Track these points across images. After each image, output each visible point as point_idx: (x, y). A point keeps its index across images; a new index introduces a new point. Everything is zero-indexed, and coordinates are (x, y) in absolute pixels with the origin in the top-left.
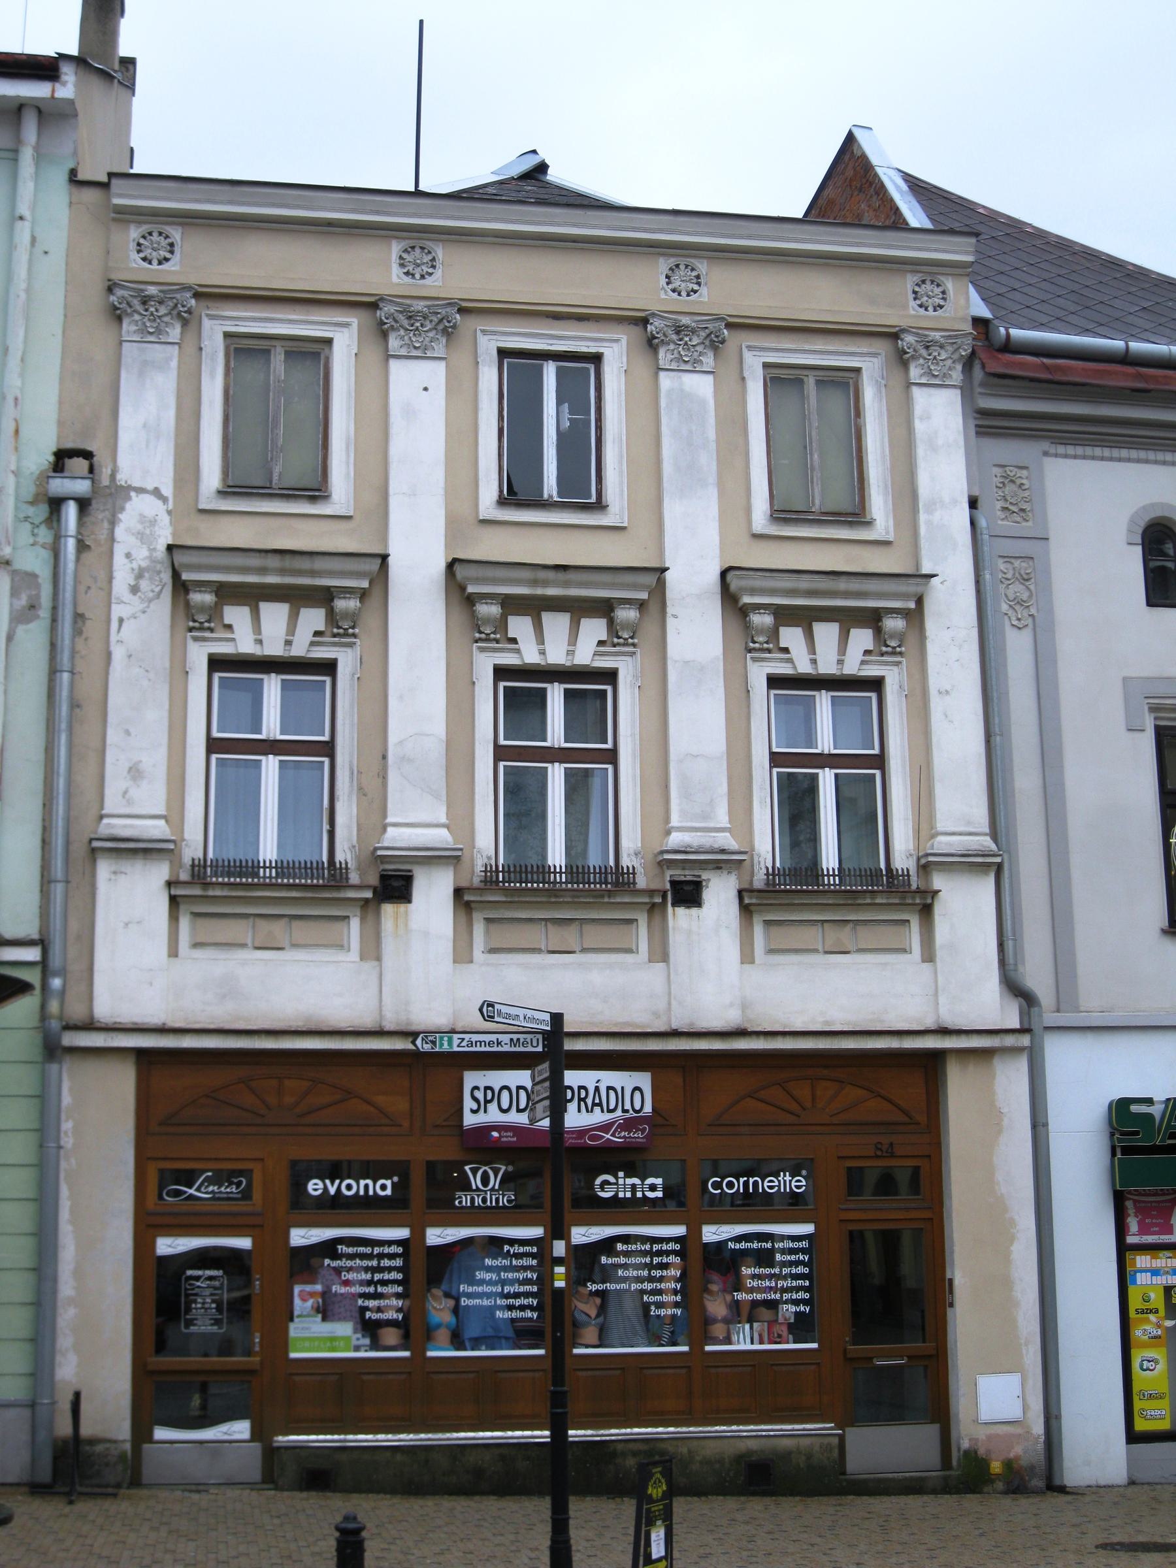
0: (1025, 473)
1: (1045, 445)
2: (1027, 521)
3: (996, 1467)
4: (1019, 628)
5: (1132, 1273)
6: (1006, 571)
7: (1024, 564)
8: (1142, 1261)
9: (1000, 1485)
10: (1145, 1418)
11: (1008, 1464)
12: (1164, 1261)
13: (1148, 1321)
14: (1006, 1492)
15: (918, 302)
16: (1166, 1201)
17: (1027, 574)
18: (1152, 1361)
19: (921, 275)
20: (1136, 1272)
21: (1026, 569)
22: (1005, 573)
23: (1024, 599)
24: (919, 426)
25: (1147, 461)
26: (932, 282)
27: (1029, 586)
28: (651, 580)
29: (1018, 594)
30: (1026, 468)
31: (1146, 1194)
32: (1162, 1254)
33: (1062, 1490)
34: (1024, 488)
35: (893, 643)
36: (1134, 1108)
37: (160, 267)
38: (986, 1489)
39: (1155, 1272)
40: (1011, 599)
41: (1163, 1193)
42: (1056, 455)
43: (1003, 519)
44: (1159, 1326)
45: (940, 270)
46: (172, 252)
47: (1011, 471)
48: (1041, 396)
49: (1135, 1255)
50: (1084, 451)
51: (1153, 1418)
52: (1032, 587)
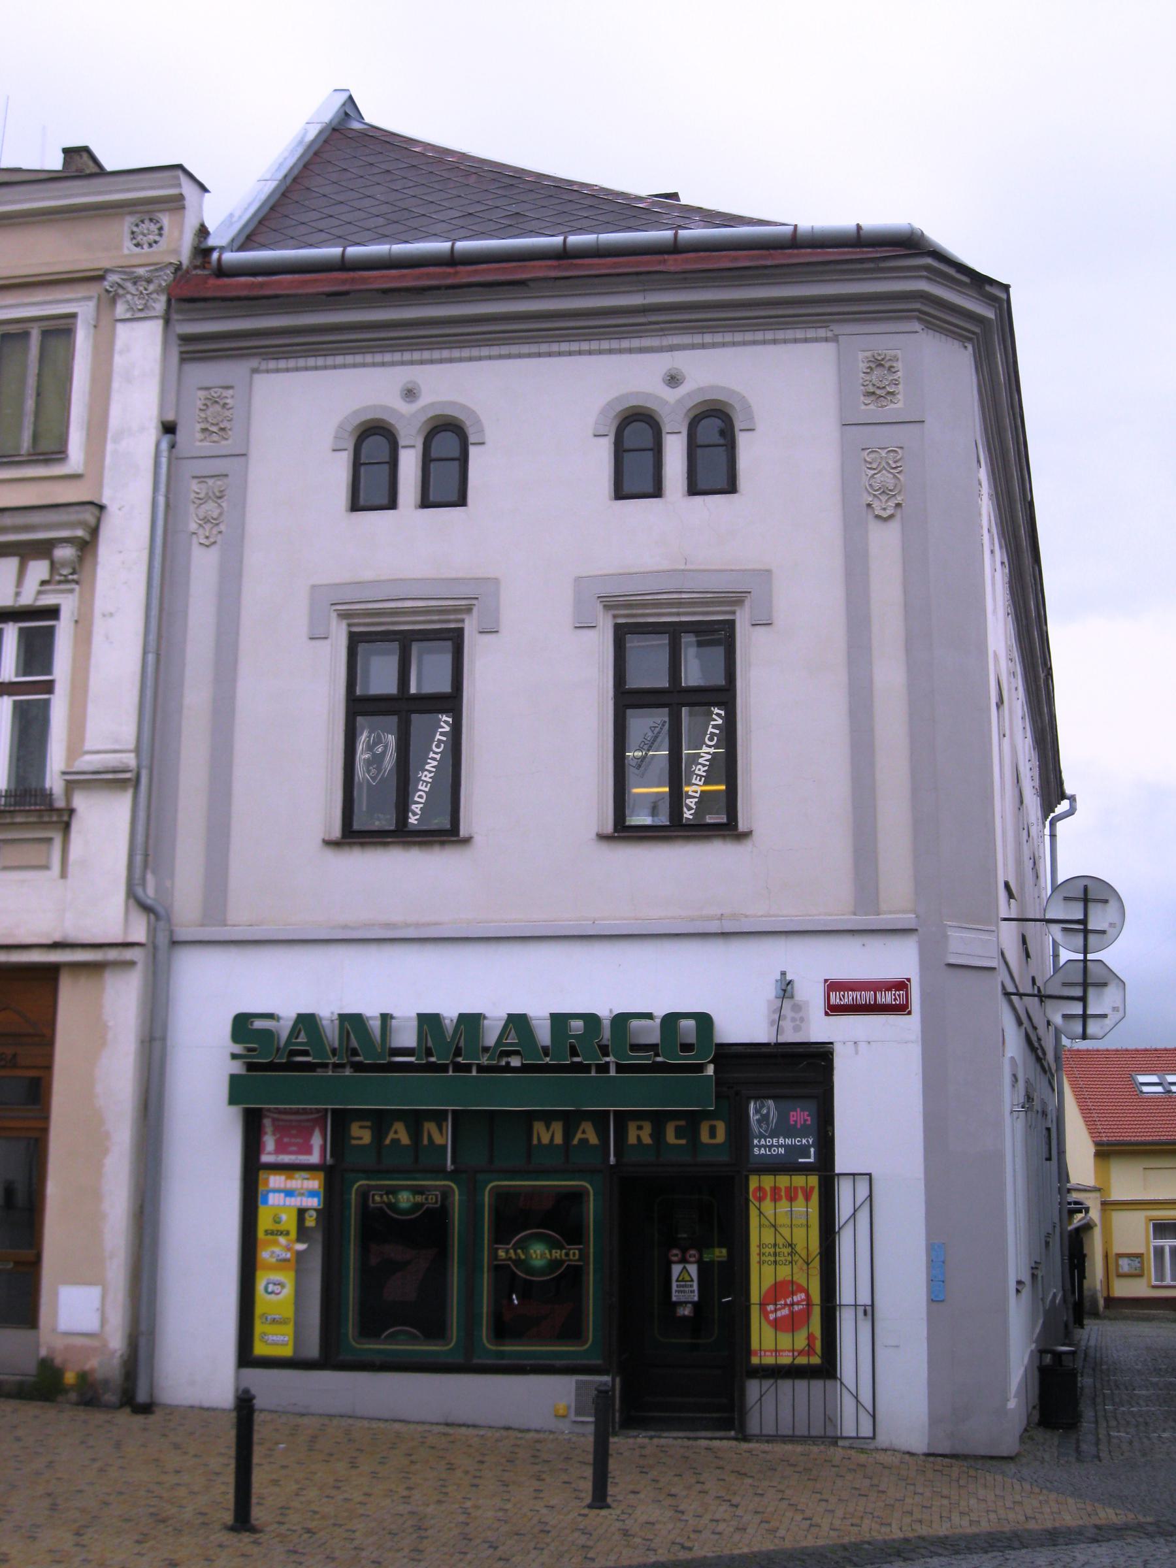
0: (230, 392)
1: (254, 363)
2: (227, 439)
3: (70, 1377)
4: (207, 546)
5: (264, 1193)
6: (198, 491)
7: (219, 483)
8: (276, 1180)
9: (73, 1396)
10: (266, 1342)
11: (83, 1377)
12: (299, 1182)
13: (277, 1243)
14: (78, 1404)
15: (135, 242)
16: (308, 1120)
17: (221, 491)
18: (279, 1284)
19: (139, 215)
20: (268, 1192)
21: (220, 486)
22: (198, 493)
23: (215, 517)
24: (118, 360)
25: (364, 365)
26: (151, 220)
27: (222, 504)
28: (89, 516)
29: (210, 513)
30: (230, 387)
31: (285, 1112)
32: (298, 1175)
33: (146, 1409)
34: (228, 407)
35: (65, 572)
36: (258, 1024)
37: (151, 249)
38: (60, 1398)
39: (289, 1193)
40: (201, 518)
41: (305, 1112)
42: (268, 371)
43: (201, 441)
44: (288, 1249)
45: (157, 207)
46: (160, 235)
47: (216, 392)
48: (681, 286)
49: (269, 1174)
50: (559, 348)
51: (275, 1344)
52: (224, 505)
